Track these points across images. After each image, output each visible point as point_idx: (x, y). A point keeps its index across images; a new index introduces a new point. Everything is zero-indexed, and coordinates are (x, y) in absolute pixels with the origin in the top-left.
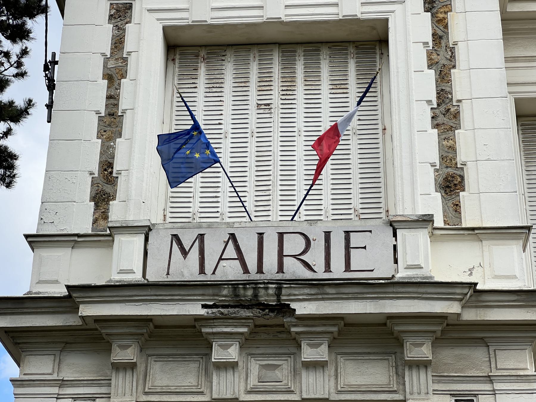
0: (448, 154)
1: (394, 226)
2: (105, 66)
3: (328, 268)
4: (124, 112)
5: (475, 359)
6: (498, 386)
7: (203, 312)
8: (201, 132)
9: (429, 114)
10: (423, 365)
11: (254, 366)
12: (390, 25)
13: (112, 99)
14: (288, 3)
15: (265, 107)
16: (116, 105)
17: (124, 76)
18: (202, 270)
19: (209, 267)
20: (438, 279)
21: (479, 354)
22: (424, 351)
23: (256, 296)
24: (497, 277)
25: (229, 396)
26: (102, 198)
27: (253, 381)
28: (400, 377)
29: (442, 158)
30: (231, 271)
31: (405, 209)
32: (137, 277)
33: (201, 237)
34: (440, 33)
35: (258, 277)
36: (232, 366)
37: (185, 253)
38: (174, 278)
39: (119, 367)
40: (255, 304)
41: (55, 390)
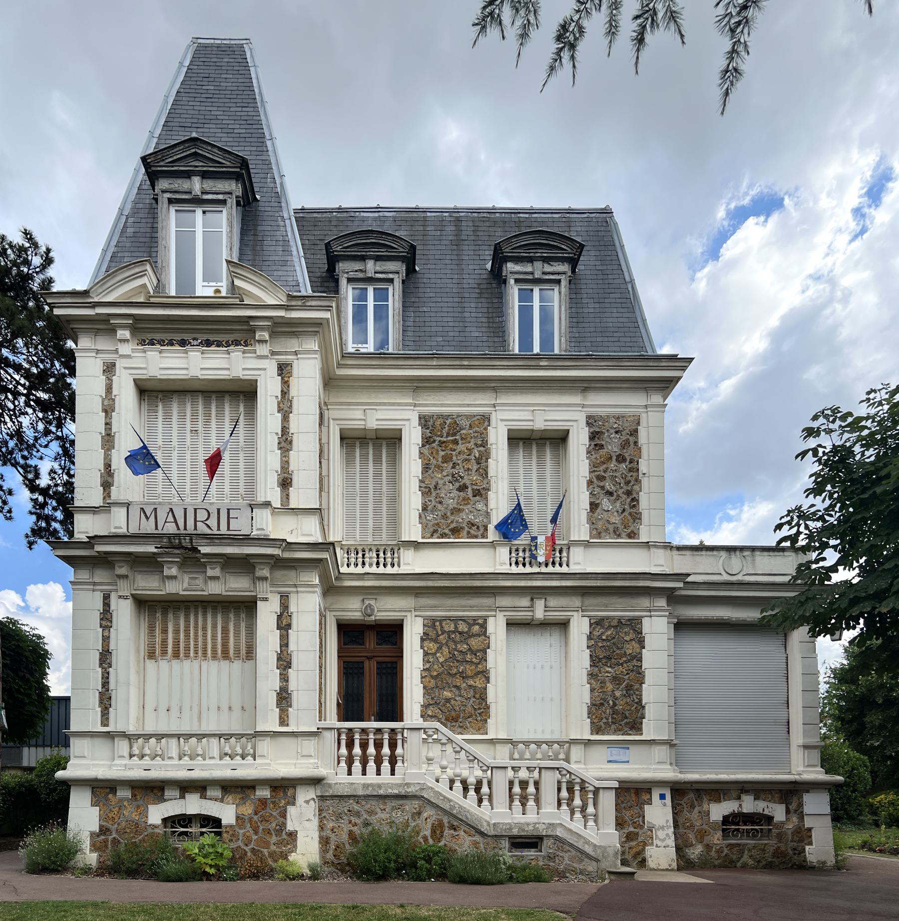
2: (103, 404)
3: (219, 529)
5: (290, 576)
6: (299, 589)
7: (155, 550)
9: (277, 441)
11: (186, 578)
13: (108, 424)
15: (195, 432)
16: (111, 429)
17: (113, 411)
18: (156, 528)
19: (160, 527)
21: (292, 573)
22: (266, 572)
23: (180, 543)
24: (304, 535)
26: (107, 485)
27: (186, 585)
28: (254, 583)
29: (282, 468)
30: (171, 528)
32: (123, 530)
34: (285, 390)
35: (184, 532)
36: (174, 578)
37: (147, 518)
39: (120, 577)
40: (180, 547)
41: (92, 587)
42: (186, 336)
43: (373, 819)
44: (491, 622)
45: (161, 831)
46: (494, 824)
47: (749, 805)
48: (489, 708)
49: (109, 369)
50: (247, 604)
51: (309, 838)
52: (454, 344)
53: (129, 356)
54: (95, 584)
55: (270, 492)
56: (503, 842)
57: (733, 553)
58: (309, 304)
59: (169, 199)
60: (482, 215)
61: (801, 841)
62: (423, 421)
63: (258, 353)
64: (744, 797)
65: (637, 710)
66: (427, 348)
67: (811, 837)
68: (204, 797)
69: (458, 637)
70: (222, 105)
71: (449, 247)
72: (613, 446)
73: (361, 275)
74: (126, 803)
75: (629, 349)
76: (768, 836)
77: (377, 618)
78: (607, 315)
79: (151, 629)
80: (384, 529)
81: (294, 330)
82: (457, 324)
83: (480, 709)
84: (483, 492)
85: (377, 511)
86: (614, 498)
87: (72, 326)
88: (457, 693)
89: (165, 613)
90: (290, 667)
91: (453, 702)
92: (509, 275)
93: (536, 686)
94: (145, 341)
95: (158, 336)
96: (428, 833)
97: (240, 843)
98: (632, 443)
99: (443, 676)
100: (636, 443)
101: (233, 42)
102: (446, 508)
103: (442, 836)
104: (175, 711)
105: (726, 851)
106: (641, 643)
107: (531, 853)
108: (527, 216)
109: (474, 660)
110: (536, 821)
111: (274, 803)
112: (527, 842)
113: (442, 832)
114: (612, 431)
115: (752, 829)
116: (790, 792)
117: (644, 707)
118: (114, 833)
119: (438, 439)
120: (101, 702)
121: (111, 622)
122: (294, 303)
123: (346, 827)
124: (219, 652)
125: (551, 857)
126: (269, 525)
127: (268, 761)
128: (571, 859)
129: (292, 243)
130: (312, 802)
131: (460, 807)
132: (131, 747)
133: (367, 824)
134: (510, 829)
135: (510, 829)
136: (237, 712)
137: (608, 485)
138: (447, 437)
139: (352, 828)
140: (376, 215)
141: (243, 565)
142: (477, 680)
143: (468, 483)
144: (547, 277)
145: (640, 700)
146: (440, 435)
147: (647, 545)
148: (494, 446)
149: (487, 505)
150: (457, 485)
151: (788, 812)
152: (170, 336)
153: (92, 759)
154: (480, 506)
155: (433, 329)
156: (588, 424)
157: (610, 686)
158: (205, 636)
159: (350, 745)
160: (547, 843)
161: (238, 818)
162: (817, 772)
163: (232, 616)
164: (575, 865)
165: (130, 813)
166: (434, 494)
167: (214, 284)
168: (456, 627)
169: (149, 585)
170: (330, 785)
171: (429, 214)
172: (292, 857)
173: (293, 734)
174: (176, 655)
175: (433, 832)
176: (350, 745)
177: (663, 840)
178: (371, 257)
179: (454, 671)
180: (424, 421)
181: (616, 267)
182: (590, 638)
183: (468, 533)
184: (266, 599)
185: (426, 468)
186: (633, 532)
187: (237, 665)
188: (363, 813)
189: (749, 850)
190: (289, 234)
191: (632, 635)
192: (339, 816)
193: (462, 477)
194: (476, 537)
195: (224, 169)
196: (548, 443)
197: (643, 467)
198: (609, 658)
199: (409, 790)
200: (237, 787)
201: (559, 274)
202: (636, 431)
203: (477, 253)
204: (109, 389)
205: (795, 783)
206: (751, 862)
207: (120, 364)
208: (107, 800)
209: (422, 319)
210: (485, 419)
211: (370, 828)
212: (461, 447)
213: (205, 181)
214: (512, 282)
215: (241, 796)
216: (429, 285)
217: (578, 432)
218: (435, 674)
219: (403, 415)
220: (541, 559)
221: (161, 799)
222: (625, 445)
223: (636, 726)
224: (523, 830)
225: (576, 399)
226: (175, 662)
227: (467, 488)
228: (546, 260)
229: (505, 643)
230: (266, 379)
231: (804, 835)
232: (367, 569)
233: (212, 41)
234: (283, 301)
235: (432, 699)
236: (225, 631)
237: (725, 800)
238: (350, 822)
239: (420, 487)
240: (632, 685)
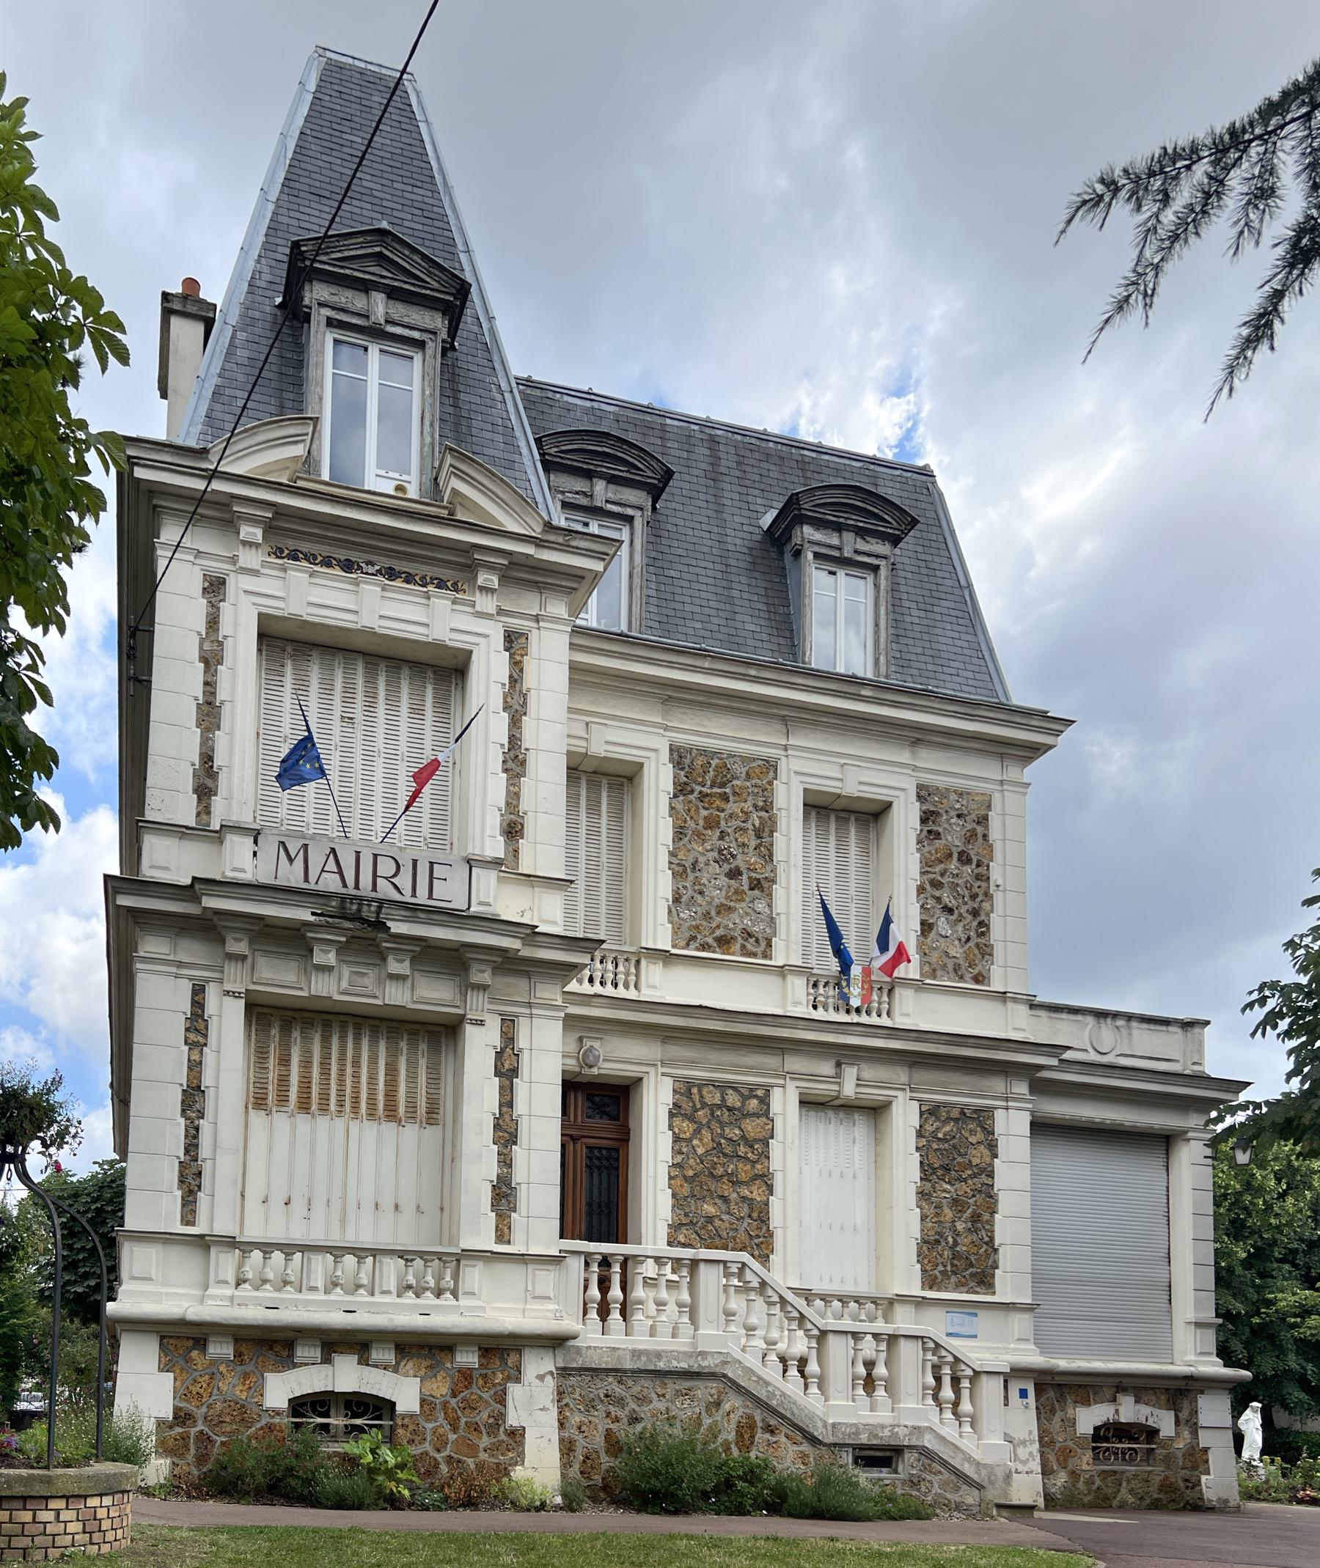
0: (513, 798)
1: (470, 863)
2: (201, 648)
3: (414, 895)
4: (222, 702)
5: (519, 987)
6: (535, 1011)
7: (312, 918)
8: (314, 745)
9: (501, 758)
10: (483, 988)
11: (346, 971)
12: (474, 657)
13: (210, 686)
14: (382, 613)
16: (214, 694)
17: (220, 662)
18: (306, 880)
19: (312, 878)
20: (503, 918)
21: (522, 983)
23: (359, 910)
25: (324, 994)
27: (344, 985)
29: (508, 804)
30: (331, 883)
31: (474, 849)
33: (306, 846)
35: (355, 892)
36: (328, 969)
37: (291, 860)
38: (280, 882)
39: (231, 957)
40: (357, 918)
41: (174, 970)
42: (355, 556)
43: (644, 1411)
44: (776, 1095)
45: (287, 1420)
46: (834, 1425)
47: (1128, 1411)
48: (771, 1236)
49: (215, 587)
50: (430, 1028)
51: (545, 1440)
52: (719, 636)
53: (255, 573)
54: (180, 964)
56: (844, 1455)
57: (1102, 1020)
58: (574, 543)
59: (328, 318)
60: (747, 440)
61: (1195, 1468)
62: (675, 755)
63: (478, 608)
64: (1121, 1398)
65: (988, 1256)
66: (680, 636)
67: (1207, 1461)
68: (364, 1361)
70: (379, 174)
71: (703, 481)
72: (953, 837)
73: (584, 501)
74: (223, 1368)
75: (973, 690)
76: (1148, 1460)
77: (602, 1072)
78: (936, 631)
79: (261, 1055)
81: (539, 579)
82: (722, 606)
83: (758, 1236)
84: (766, 885)
86: (953, 918)
87: (155, 502)
88: (724, 1207)
89: (286, 1030)
90: (515, 1143)
91: (717, 1223)
92: (806, 545)
93: (840, 1202)
94: (315, 558)
95: (305, 547)
96: (732, 1436)
97: (427, 1447)
98: (980, 836)
100: (985, 836)
101: (384, 71)
102: (710, 903)
103: (752, 1443)
104: (298, 1206)
105: (1098, 1482)
106: (993, 1148)
107: (884, 1474)
108: (814, 455)
109: (750, 1155)
110: (891, 1422)
111: (485, 1376)
112: (879, 1456)
113: (753, 1437)
114: (953, 813)
115: (1130, 1449)
116: (1179, 1392)
117: (996, 1250)
118: (200, 1422)
119: (698, 788)
120: (182, 1180)
121: (206, 1036)
122: (552, 538)
123: (602, 1425)
124: (381, 1106)
125: (913, 1482)
126: (510, 903)
127: (480, 1303)
128: (944, 1485)
129: (518, 433)
130: (549, 1378)
131: (783, 1394)
132: (240, 1265)
133: (634, 1420)
134: (857, 1433)
135: (857, 1433)
136: (408, 1214)
137: (947, 898)
138: (712, 787)
139: (611, 1426)
140: (588, 404)
141: (450, 961)
142: (754, 1188)
143: (743, 867)
144: (860, 558)
145: (992, 1239)
146: (702, 781)
147: (1003, 996)
148: (784, 813)
149: (770, 906)
150: (726, 867)
151: (1177, 1423)
152: (326, 550)
153: (165, 1284)
154: (761, 906)
155: (687, 608)
156: (920, 798)
157: (948, 1214)
158: (356, 1076)
159: (604, 1285)
160: (910, 1457)
161: (423, 1401)
162: (1214, 1364)
163: (403, 1045)
164: (948, 1496)
165: (230, 1385)
166: (691, 876)
167: (396, 475)
168: (723, 1099)
169: (280, 977)
170: (578, 1350)
171: (668, 421)
172: (518, 1473)
173: (523, 1259)
174: (304, 1106)
175: (739, 1434)
176: (604, 1285)
177: (1025, 1462)
178: (601, 476)
179: (720, 1171)
180: (679, 756)
181: (944, 560)
182: (920, 1134)
183: (743, 947)
184: (481, 1023)
185: (679, 833)
186: (980, 974)
187: (410, 1133)
188: (629, 1400)
189: (1128, 1481)
190: (513, 417)
191: (980, 1136)
192: (590, 1405)
193: (734, 856)
194: (754, 955)
195: (428, 292)
196: (853, 818)
197: (996, 874)
198: (947, 1169)
199: (705, 1363)
200: (422, 1347)
201: (877, 556)
202: (986, 818)
203: (744, 498)
204: (213, 622)
205: (1189, 1378)
206: (1131, 1499)
207: (236, 584)
208: (188, 1360)
209: (669, 589)
210: (770, 767)
211: (639, 1427)
212: (732, 807)
213: (391, 302)
214: (810, 556)
215: (428, 1363)
216: (677, 536)
217: (906, 808)
218: (691, 1173)
219: (644, 739)
220: (855, 1002)
222: (970, 837)
223: (985, 1280)
224: (876, 1436)
225: (904, 756)
226: (301, 1119)
227: (740, 874)
228: (861, 533)
229: (797, 1131)
230: (488, 653)
231: (1197, 1459)
232: (597, 989)
233: (350, 61)
234: (537, 530)
235: (686, 1215)
236: (392, 1071)
237: (1096, 1403)
238: (608, 1415)
239: (670, 863)
240: (979, 1215)
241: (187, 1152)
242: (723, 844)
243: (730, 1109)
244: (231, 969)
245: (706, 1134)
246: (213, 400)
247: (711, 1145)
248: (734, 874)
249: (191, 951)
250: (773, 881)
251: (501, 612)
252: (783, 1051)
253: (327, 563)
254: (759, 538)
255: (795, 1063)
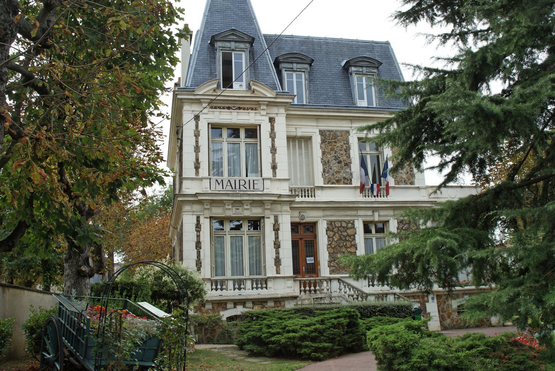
0: (274, 160)
5: (279, 207)
9: (270, 150)
11: (234, 209)
19: (224, 188)
27: (234, 212)
33: (222, 180)
37: (219, 184)
39: (205, 209)
53: (207, 114)
55: (267, 172)
69: (342, 229)
80: (305, 178)
85: (301, 170)
99: (337, 247)
141: (261, 203)
147: (418, 188)
150: (337, 161)
168: (341, 225)
173: (284, 278)
179: (342, 245)
180: (322, 133)
184: (269, 218)
185: (324, 153)
194: (347, 184)
207: (202, 117)
210: (348, 132)
212: (338, 145)
218: (333, 246)
219: (312, 129)
221: (225, 309)
241: (198, 258)
242: (336, 155)
243: (343, 227)
244: (206, 211)
245: (337, 235)
246: (194, 71)
247: (339, 238)
248: (340, 162)
249: (196, 207)
250: (351, 163)
251: (267, 114)
252: (357, 210)
253: (224, 108)
254: (341, 69)
255: (361, 213)
